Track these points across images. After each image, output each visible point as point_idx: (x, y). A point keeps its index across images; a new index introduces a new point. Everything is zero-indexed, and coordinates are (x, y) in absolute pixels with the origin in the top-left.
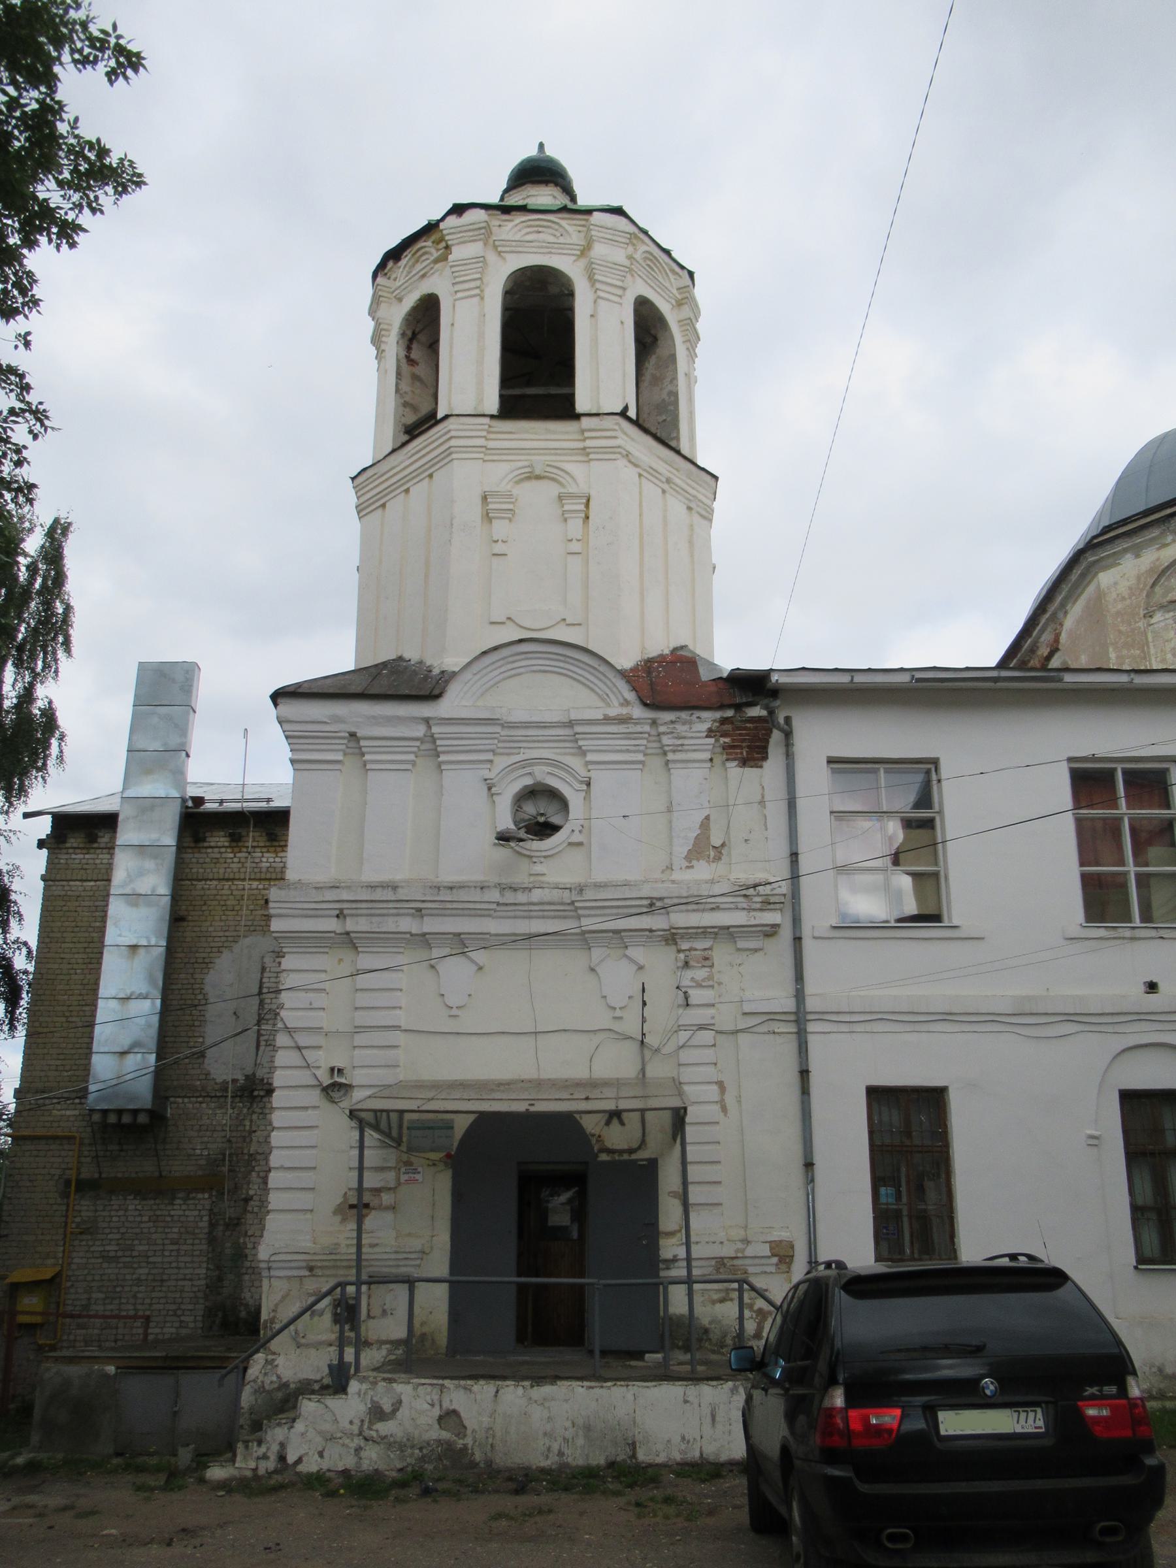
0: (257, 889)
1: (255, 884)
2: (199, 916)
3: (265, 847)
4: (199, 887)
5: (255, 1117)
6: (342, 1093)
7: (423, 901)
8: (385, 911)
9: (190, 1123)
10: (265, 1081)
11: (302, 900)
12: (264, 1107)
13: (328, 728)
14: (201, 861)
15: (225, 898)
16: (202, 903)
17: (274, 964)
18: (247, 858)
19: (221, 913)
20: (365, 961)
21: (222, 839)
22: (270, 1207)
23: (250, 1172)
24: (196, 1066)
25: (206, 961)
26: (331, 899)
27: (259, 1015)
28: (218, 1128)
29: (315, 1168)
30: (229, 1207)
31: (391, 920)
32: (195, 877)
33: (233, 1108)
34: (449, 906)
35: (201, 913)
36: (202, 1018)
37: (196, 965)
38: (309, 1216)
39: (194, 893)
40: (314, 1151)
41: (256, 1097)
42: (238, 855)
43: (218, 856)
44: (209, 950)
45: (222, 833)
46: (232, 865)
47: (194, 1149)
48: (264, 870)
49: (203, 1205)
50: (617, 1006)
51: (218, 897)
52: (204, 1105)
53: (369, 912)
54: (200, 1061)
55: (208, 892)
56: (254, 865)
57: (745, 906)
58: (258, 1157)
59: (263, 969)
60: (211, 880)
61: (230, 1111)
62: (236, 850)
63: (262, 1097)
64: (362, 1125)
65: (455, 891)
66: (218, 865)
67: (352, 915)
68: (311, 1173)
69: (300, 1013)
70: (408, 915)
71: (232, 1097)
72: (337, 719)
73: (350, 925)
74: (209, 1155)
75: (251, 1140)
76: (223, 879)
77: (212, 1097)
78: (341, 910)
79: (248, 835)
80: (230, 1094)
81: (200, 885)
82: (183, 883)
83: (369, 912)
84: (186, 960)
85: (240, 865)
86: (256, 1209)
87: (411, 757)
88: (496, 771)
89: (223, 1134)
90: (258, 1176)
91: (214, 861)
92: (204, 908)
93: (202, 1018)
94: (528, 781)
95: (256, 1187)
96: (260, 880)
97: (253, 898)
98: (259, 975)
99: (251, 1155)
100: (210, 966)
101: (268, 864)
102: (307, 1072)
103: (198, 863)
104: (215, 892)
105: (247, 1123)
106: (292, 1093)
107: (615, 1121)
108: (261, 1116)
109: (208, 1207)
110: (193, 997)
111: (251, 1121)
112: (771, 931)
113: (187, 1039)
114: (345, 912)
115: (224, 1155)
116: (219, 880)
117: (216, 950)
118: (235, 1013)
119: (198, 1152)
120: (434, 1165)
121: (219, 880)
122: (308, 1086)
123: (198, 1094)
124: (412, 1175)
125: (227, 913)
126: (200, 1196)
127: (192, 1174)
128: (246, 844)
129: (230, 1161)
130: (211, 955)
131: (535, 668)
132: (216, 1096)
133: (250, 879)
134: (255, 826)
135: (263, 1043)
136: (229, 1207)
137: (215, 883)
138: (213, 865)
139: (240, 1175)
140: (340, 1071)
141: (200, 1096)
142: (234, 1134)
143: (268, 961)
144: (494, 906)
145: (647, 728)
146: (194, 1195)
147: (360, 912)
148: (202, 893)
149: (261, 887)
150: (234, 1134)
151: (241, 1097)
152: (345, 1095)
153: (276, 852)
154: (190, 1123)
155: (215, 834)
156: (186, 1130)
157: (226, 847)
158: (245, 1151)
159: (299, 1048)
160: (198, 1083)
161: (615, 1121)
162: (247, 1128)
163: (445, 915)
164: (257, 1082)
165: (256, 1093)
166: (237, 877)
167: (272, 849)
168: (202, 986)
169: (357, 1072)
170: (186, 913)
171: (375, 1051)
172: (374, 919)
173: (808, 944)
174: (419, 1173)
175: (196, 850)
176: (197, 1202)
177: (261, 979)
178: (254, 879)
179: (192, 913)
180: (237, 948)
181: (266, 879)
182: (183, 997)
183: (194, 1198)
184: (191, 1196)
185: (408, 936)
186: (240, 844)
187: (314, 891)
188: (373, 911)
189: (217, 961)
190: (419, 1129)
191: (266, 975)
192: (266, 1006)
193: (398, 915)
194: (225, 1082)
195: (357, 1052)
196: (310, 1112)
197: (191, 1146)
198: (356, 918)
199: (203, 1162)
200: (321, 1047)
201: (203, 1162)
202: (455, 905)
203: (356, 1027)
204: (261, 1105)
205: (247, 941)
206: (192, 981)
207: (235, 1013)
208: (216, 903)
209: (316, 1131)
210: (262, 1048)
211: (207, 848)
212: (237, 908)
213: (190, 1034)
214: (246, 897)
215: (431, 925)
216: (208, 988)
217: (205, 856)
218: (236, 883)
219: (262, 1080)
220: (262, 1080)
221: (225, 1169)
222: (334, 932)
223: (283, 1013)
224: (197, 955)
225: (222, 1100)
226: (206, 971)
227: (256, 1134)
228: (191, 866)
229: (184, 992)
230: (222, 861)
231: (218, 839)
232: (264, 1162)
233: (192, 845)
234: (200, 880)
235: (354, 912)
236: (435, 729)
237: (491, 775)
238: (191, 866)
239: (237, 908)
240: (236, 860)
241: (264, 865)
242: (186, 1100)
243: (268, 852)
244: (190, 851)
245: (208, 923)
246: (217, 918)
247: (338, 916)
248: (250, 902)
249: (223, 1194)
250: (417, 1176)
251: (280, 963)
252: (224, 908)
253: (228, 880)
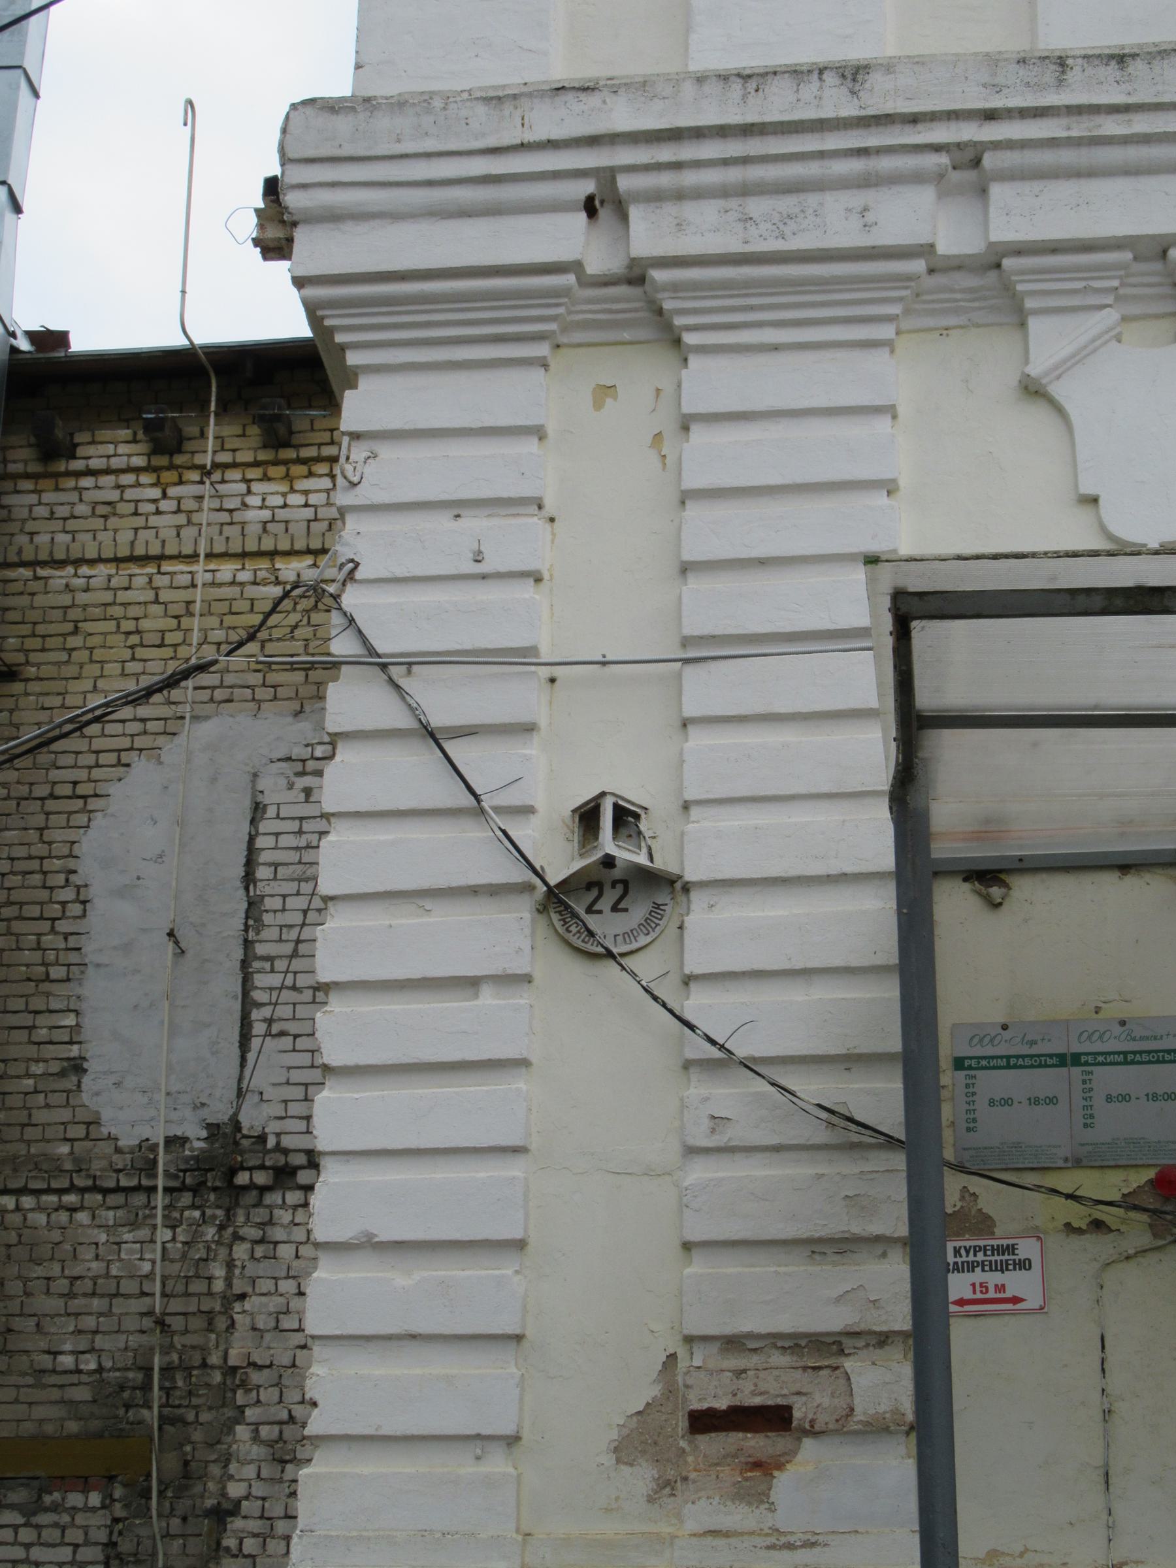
0: (233, 583)
1: (226, 570)
2: (58, 664)
3: (256, 464)
4: (57, 583)
5: (241, 1251)
6: (638, 912)
7: (990, 115)
8: (812, 169)
9: (39, 1271)
10: (271, 1142)
11: (430, 145)
12: (271, 1222)
14: (62, 511)
15: (134, 611)
16: (69, 627)
17: (291, 796)
18: (200, 498)
19: (127, 654)
21: (123, 449)
22: (317, 1424)
23: (229, 1427)
24: (55, 1099)
25: (81, 790)
26: (557, 134)
27: (247, 944)
28: (129, 1287)
29: (520, 1245)
30: (167, 1535)
31: (835, 204)
32: (43, 556)
33: (173, 1228)
34: (1111, 126)
35: (64, 656)
36: (73, 957)
37: (51, 805)
38: (498, 1464)
39: (39, 600)
40: (515, 1169)
41: (244, 1188)
42: (172, 491)
43: (114, 495)
44: (90, 759)
45: (125, 433)
46: (154, 520)
47: (55, 1354)
49: (86, 1529)
51: (117, 611)
52: (82, 1217)
53: (734, 175)
54: (70, 1082)
55: (82, 598)
56: (224, 517)
58: (256, 1377)
59: (258, 810)
60: (91, 562)
61: (164, 1234)
62: (169, 476)
63: (263, 1190)
65: (1137, 68)
66: (113, 522)
67: (656, 197)
68: (506, 1269)
70: (917, 178)
71: (167, 1190)
74: (100, 1369)
75: (233, 1324)
76: (132, 559)
77: (105, 1192)
78: (608, 176)
79: (203, 435)
80: (160, 1183)
81: (60, 577)
82: (11, 574)
83: (734, 175)
84: (24, 791)
85: (181, 519)
86: (250, 1546)
89: (142, 1304)
90: (256, 1438)
91: (102, 510)
92: (73, 642)
93: (73, 957)
95: (250, 1471)
96: (244, 555)
97: (223, 607)
98: (246, 827)
99: (234, 1369)
100: (93, 804)
101: (266, 514)
102: (474, 833)
103: (52, 516)
104: (107, 597)
105: (218, 1271)
106: (405, 919)
108: (259, 1251)
109: (102, 1536)
110: (44, 895)
111: (230, 1265)
113: (27, 1020)
114: (625, 183)
115: (148, 1370)
116: (117, 560)
117: (111, 758)
118: (171, 934)
119: (67, 1361)
120: (1098, 1225)
121: (117, 560)
122: (474, 891)
123: (62, 1183)
124: (994, 1278)
125: (140, 653)
126: (75, 1499)
127: (49, 1429)
128: (198, 459)
129: (167, 1391)
130: (96, 773)
132: (118, 1189)
133: (210, 556)
134: (224, 408)
135: (259, 1028)
136: (167, 1535)
137: (103, 570)
138: (98, 523)
139: (197, 1436)
140: (625, 818)
141: (72, 1189)
142: (175, 1305)
143: (273, 788)
146: (57, 1496)
147: (690, 178)
148: (66, 599)
149: (245, 576)
150: (175, 1305)
151: (195, 1190)
152: (650, 923)
153: (288, 477)
154: (39, 1271)
155: (104, 434)
156: (27, 1294)
157: (137, 470)
158: (214, 1359)
159: (432, 735)
160: (65, 1149)
162: (219, 1286)
163: (1090, 173)
164: (245, 1143)
165: (242, 1178)
167: (276, 471)
168: (71, 864)
169: (703, 822)
170: (21, 658)
172: (757, 206)
174: (1025, 1265)
175: (44, 484)
176: (65, 1518)
177: (251, 840)
178: (225, 555)
179: (34, 657)
180: (172, 751)
181: (260, 554)
182: (16, 896)
183: (55, 1508)
184: (47, 1499)
185: (918, 266)
186: (179, 460)
187: (481, 109)
188: (756, 173)
189: (113, 789)
190: (1010, 1063)
191: (263, 827)
192: (267, 918)
193: (866, 182)
194: (147, 1147)
195: (699, 739)
196: (488, 997)
197: (43, 1345)
198: (670, 209)
199: (82, 1394)
200: (529, 729)
201: (82, 1394)
202: (1141, 124)
203: (686, 642)
204: (260, 1215)
205: (206, 730)
206: (39, 849)
207: (171, 934)
208: (111, 626)
209: (520, 1084)
210: (255, 1043)
211: (78, 474)
212: (170, 638)
213: (38, 1003)
214: (197, 607)
216: (88, 869)
217: (74, 497)
218: (166, 567)
219: (262, 1138)
220: (262, 1138)
221: (152, 1416)
222: (575, 267)
223: (351, 599)
224: (54, 775)
225: (139, 1199)
226: (82, 819)
227: (247, 1305)
228: (30, 526)
229: (16, 880)
230: (123, 508)
231: (110, 449)
232: (274, 1393)
233: (34, 468)
234: (61, 564)
235: (665, 180)
238: (30, 526)
239: (170, 638)
240: (164, 505)
241: (251, 515)
242: (27, 1201)
243: (266, 478)
244: (28, 485)
245: (87, 685)
246: (113, 669)
247: (590, 207)
248: (214, 621)
249: (146, 1494)
250: (1015, 1282)
251: (308, 792)
252: (134, 639)
253: (145, 559)
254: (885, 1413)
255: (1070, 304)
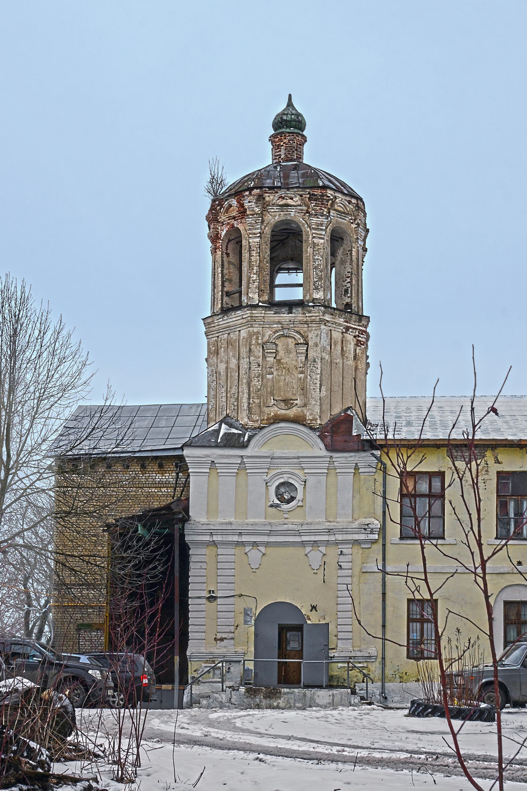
13: (203, 459)
15: (139, 496)
20: (220, 551)
48: (157, 482)
50: (315, 568)
57: (364, 532)
64: (57, 562)
69: (197, 570)
72: (208, 456)
73: (215, 538)
87: (236, 471)
88: (269, 476)
94: (282, 480)
96: (156, 487)
104: (135, 493)
107: (314, 610)
112: (374, 542)
131: (285, 433)
140: (213, 591)
144: (269, 532)
145: (329, 459)
149: (156, 491)
161: (314, 610)
166: (145, 486)
169: (219, 592)
171: (225, 584)
173: (388, 546)
181: (158, 487)
215: (244, 539)
231: (134, 467)
236: (245, 460)
237: (267, 478)
240: (143, 477)
243: (159, 473)
254: (340, 413)
255: (6, 453)
